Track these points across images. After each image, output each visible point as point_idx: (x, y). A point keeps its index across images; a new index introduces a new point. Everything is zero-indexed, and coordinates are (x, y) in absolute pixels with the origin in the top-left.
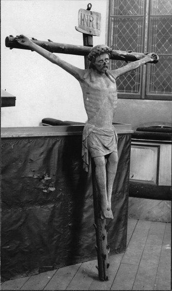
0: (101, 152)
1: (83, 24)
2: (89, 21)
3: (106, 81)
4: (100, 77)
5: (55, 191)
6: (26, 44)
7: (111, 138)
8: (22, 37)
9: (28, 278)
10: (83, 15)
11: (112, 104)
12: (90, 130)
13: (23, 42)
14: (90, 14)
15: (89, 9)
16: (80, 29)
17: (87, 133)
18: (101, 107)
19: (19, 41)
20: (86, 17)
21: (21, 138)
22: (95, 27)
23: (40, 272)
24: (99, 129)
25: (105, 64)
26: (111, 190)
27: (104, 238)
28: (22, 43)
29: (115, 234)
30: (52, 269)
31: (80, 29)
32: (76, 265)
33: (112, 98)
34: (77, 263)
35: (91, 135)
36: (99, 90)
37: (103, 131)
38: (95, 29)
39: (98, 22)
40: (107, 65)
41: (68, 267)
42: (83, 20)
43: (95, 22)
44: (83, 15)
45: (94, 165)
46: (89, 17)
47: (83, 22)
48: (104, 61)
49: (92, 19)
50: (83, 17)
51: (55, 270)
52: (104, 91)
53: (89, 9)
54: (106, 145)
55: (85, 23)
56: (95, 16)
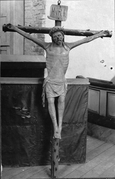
0: (50, 95)
1: (53, 14)
2: (58, 12)
3: (61, 49)
4: (57, 47)
5: (30, 117)
6: (12, 28)
7: (60, 87)
8: (10, 25)
9: (11, 168)
10: (53, 8)
11: (62, 64)
12: (47, 81)
13: (10, 27)
14: (59, 7)
15: (59, 4)
16: (50, 17)
17: (45, 82)
18: (54, 66)
19: (8, 27)
20: (56, 9)
21: (6, 84)
22: (62, 15)
23: (20, 166)
24: (52, 80)
25: (58, 38)
26: (61, 120)
27: (55, 151)
28: (10, 28)
29: (77, 150)
30: (29, 166)
31: (50, 17)
32: (46, 166)
33: (62, 61)
34: (47, 165)
35: (47, 84)
36: (53, 55)
37: (54, 82)
38: (63, 17)
39: (65, 12)
40: (59, 39)
41: (40, 166)
42: (54, 11)
43: (62, 12)
44: (53, 8)
45: (47, 103)
46: (58, 9)
47: (53, 13)
48: (57, 37)
49: (60, 11)
50: (53, 10)
51: (31, 167)
52: (56, 56)
53: (59, 4)
54: (55, 91)
55: (55, 13)
56: (63, 10)
